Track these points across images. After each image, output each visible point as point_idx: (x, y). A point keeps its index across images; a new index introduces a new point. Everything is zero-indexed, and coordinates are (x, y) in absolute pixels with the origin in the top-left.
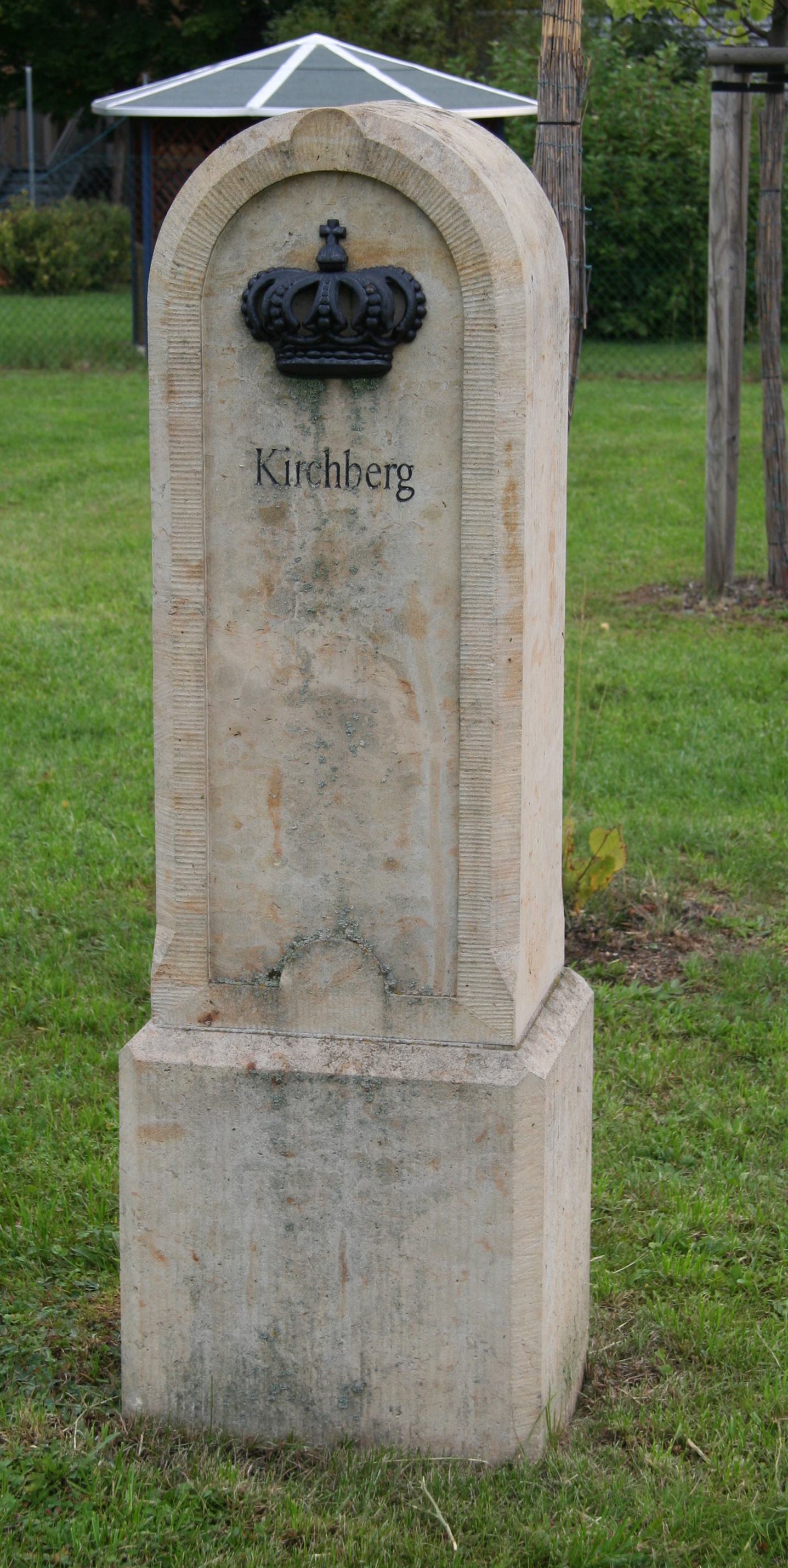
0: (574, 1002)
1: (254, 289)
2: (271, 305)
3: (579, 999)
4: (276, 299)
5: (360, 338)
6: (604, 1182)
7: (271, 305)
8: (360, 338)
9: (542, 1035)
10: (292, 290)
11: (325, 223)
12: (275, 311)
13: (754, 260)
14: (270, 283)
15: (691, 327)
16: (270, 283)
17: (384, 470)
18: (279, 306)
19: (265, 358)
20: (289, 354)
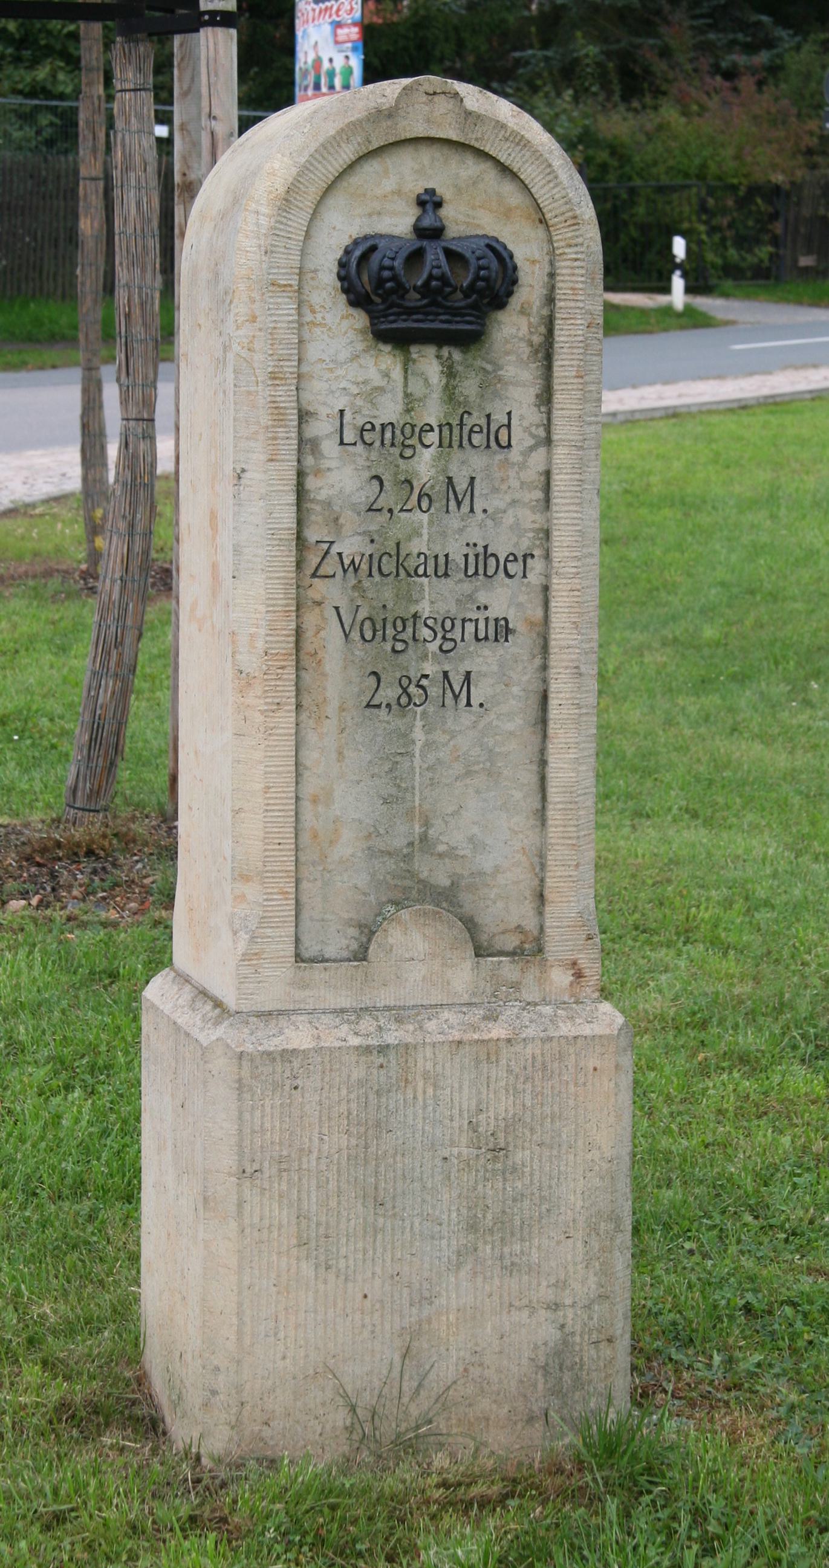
0: (199, 1023)
1: (358, 253)
2: (382, 268)
3: (202, 1029)
4: (387, 262)
5: (425, 301)
6: (132, 1151)
7: (382, 268)
8: (425, 301)
9: (176, 988)
10: (404, 254)
11: (422, 191)
12: (386, 274)
13: (107, 262)
14: (373, 249)
15: (608, 288)
16: (373, 249)
17: (520, 559)
18: (391, 268)
19: (360, 319)
20: (392, 318)
